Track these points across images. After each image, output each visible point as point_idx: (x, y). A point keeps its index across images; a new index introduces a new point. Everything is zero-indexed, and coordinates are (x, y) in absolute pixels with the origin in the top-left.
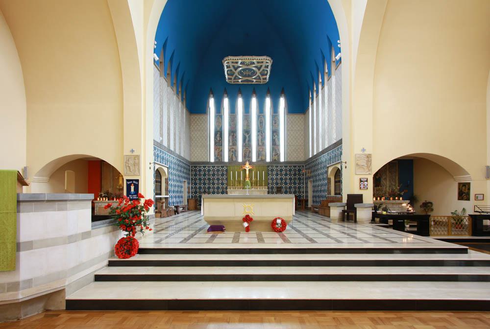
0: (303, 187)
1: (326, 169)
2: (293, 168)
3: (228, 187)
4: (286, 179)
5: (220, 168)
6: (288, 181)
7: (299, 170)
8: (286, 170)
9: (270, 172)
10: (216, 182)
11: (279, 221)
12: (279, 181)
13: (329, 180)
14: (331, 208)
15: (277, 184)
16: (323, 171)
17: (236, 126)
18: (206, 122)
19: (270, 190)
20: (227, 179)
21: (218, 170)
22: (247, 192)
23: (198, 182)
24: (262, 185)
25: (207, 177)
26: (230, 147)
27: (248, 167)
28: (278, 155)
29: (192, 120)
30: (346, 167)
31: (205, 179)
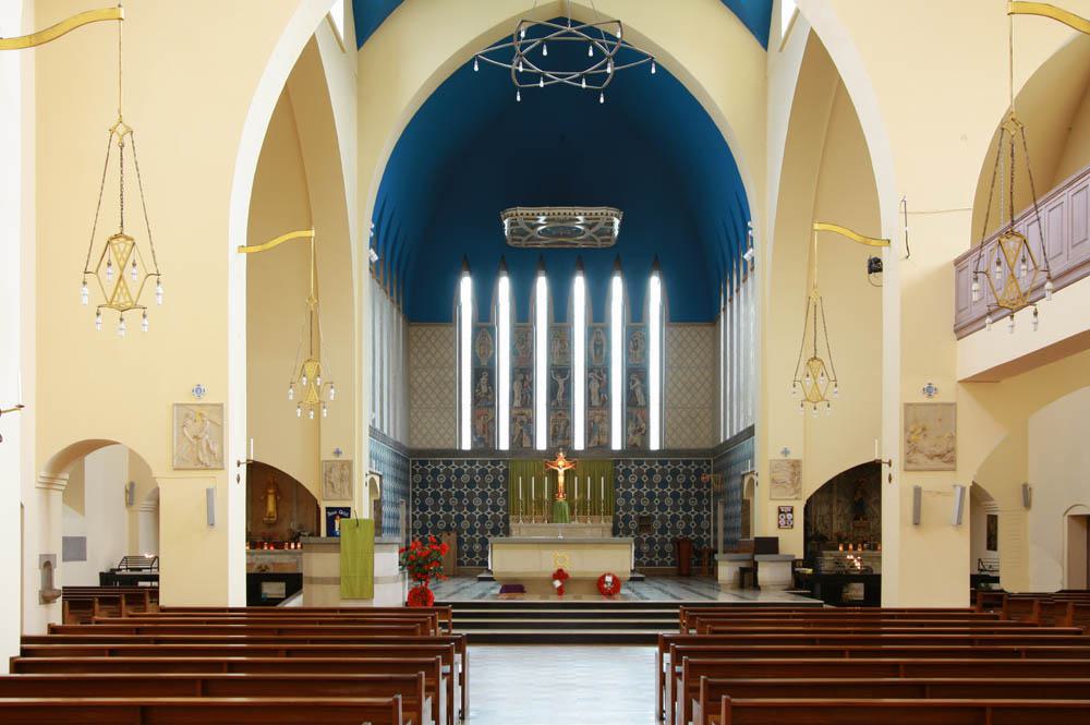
0: (709, 516)
2: (681, 467)
3: (511, 517)
4: (663, 496)
5: (489, 468)
6: (669, 501)
7: (699, 473)
8: (663, 473)
9: (621, 478)
10: (477, 502)
11: (609, 579)
12: (645, 502)
14: (760, 564)
15: (639, 508)
17: (532, 353)
18: (451, 345)
19: (621, 525)
20: (506, 495)
21: (483, 473)
22: (560, 531)
23: (429, 501)
24: (599, 514)
25: (453, 490)
26: (515, 412)
27: (561, 466)
28: (644, 433)
29: (415, 339)
31: (448, 495)
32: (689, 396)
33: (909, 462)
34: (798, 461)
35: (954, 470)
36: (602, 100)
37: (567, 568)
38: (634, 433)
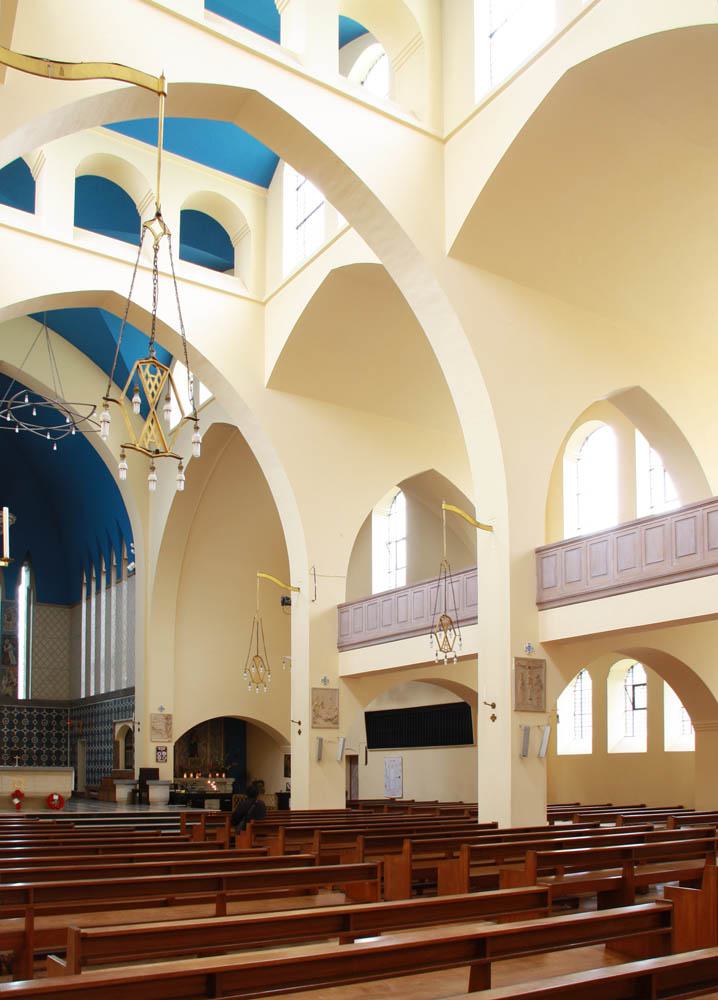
0: (66, 753)
1: (110, 727)
6: (35, 740)
7: (58, 719)
11: (56, 797)
13: (116, 744)
16: (108, 727)
30: (300, 732)
32: (51, 659)
33: (314, 723)
34: (170, 715)
35: (337, 728)
36: (55, 448)
37: (23, 789)
38: (7, 686)
